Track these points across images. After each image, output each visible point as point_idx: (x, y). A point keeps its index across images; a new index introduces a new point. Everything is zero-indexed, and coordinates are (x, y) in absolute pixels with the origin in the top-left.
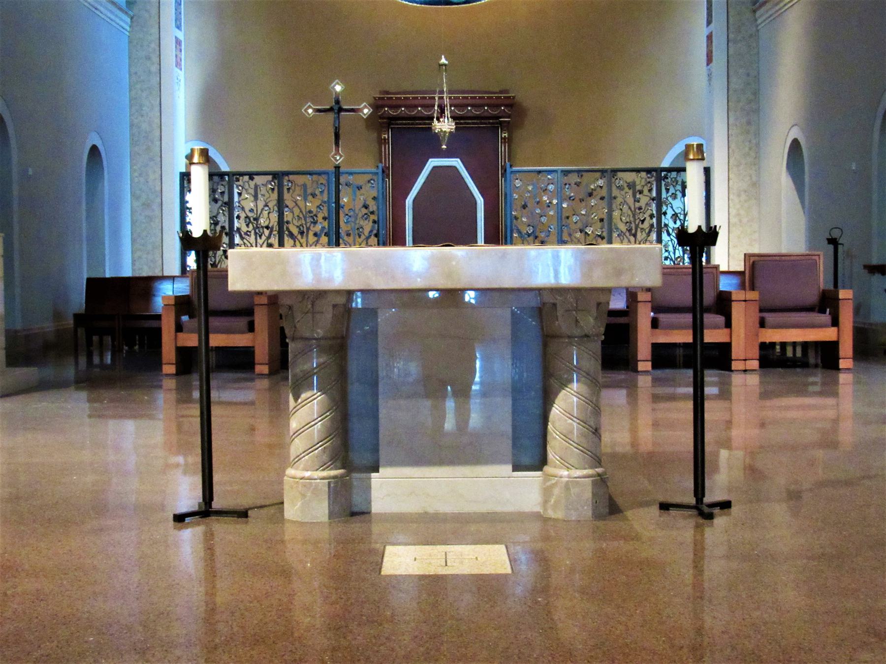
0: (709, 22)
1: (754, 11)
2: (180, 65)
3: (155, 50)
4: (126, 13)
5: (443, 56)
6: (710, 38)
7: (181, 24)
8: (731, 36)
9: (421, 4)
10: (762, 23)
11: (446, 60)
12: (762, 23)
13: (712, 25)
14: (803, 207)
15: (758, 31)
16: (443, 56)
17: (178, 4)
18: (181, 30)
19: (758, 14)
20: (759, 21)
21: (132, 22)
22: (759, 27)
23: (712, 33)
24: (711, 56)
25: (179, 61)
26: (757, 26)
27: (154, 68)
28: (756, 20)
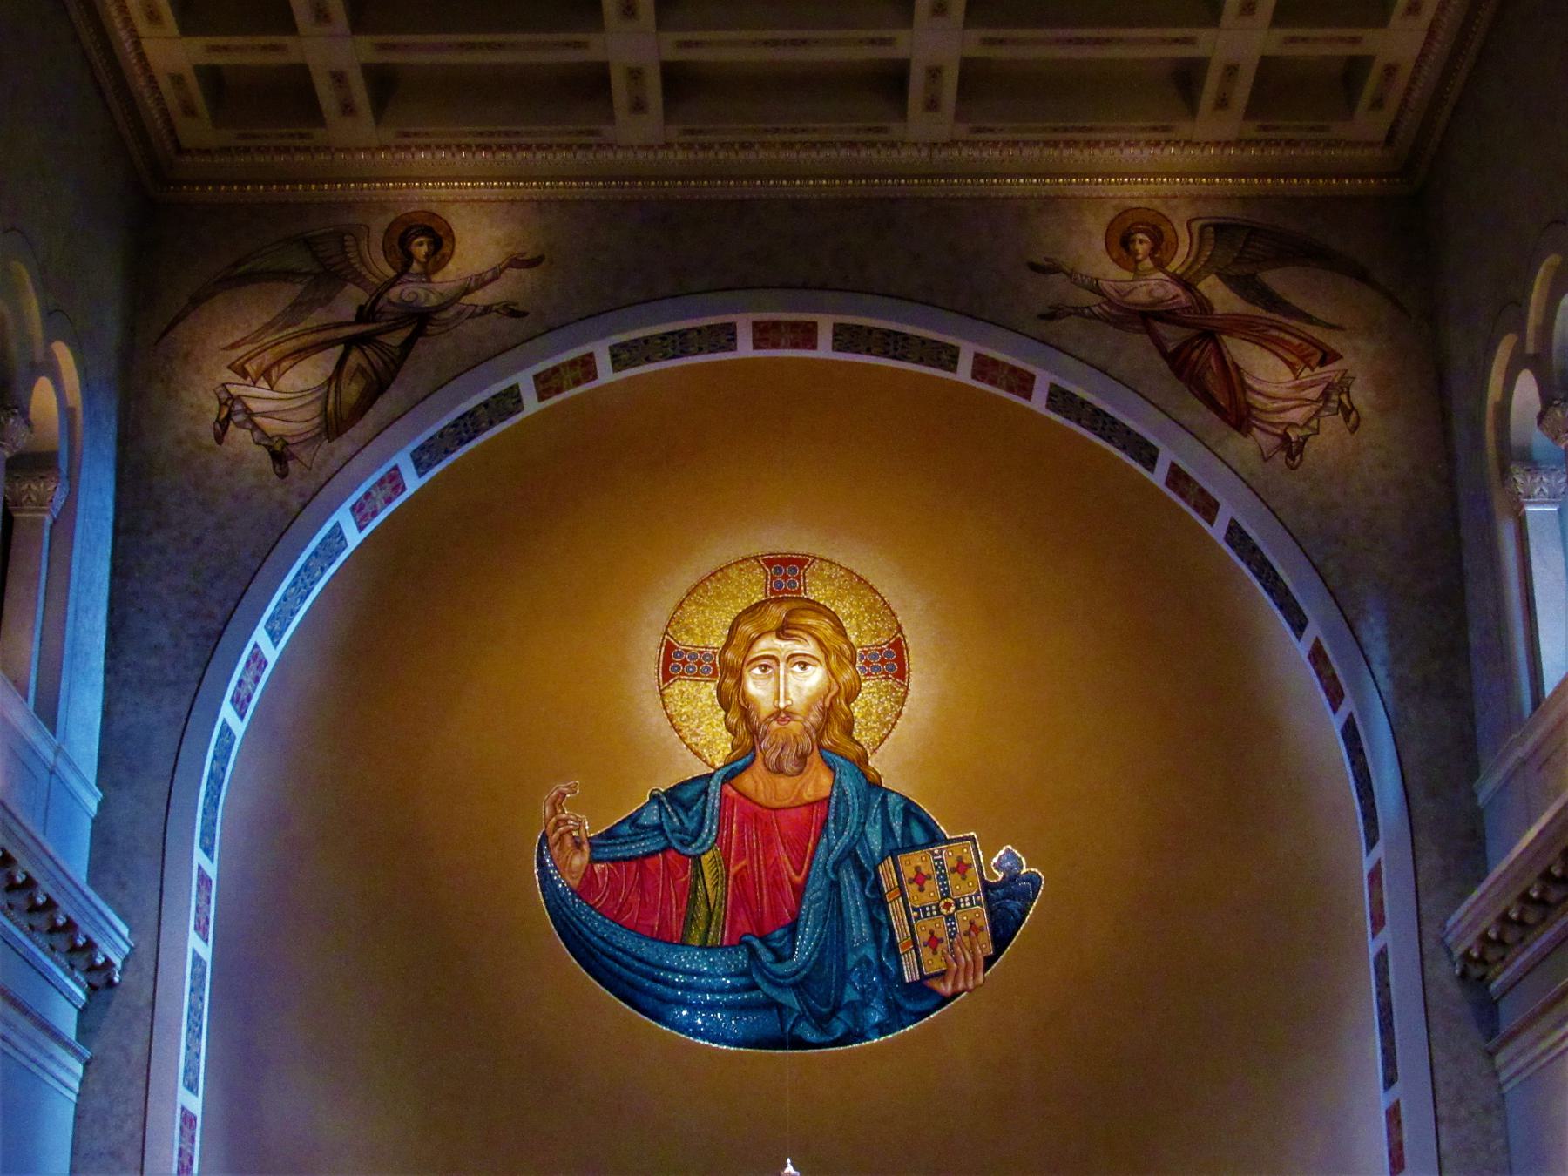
0: (1389, 1082)
1: (1491, 1055)
2: (205, 931)
3: (132, 1136)
4: (76, 1053)
5: (789, 1161)
6: (1393, 1114)
7: (197, 1080)
8: (1443, 1110)
9: (738, 1045)
10: (1512, 1077)
11: (795, 1168)
12: (1512, 1077)
13: (1398, 1086)
14: (1235, 364)
15: (1503, 1096)
16: (789, 1161)
17: (184, 1169)
18: (196, 1094)
19: (1500, 1059)
20: (1504, 1076)
21: (86, 1070)
22: (1505, 1089)
23: (1398, 1102)
24: (1401, 1157)
25: (186, 1163)
26: (1500, 1086)
27: (137, 1050)
28: (1496, 1074)
